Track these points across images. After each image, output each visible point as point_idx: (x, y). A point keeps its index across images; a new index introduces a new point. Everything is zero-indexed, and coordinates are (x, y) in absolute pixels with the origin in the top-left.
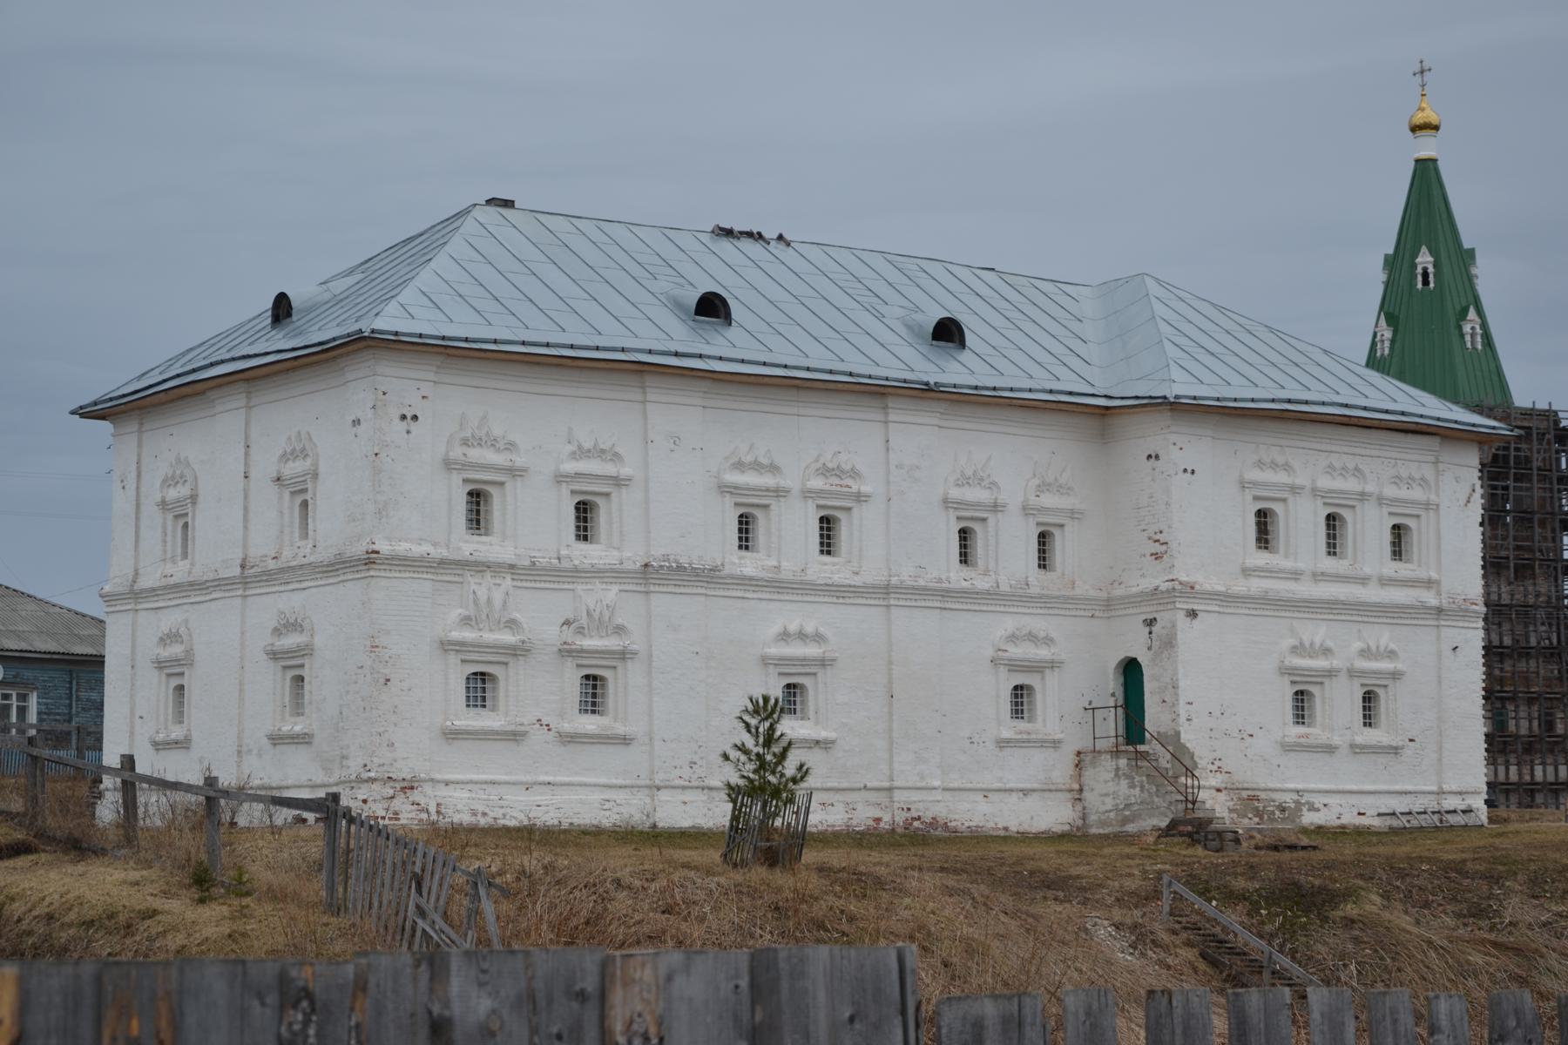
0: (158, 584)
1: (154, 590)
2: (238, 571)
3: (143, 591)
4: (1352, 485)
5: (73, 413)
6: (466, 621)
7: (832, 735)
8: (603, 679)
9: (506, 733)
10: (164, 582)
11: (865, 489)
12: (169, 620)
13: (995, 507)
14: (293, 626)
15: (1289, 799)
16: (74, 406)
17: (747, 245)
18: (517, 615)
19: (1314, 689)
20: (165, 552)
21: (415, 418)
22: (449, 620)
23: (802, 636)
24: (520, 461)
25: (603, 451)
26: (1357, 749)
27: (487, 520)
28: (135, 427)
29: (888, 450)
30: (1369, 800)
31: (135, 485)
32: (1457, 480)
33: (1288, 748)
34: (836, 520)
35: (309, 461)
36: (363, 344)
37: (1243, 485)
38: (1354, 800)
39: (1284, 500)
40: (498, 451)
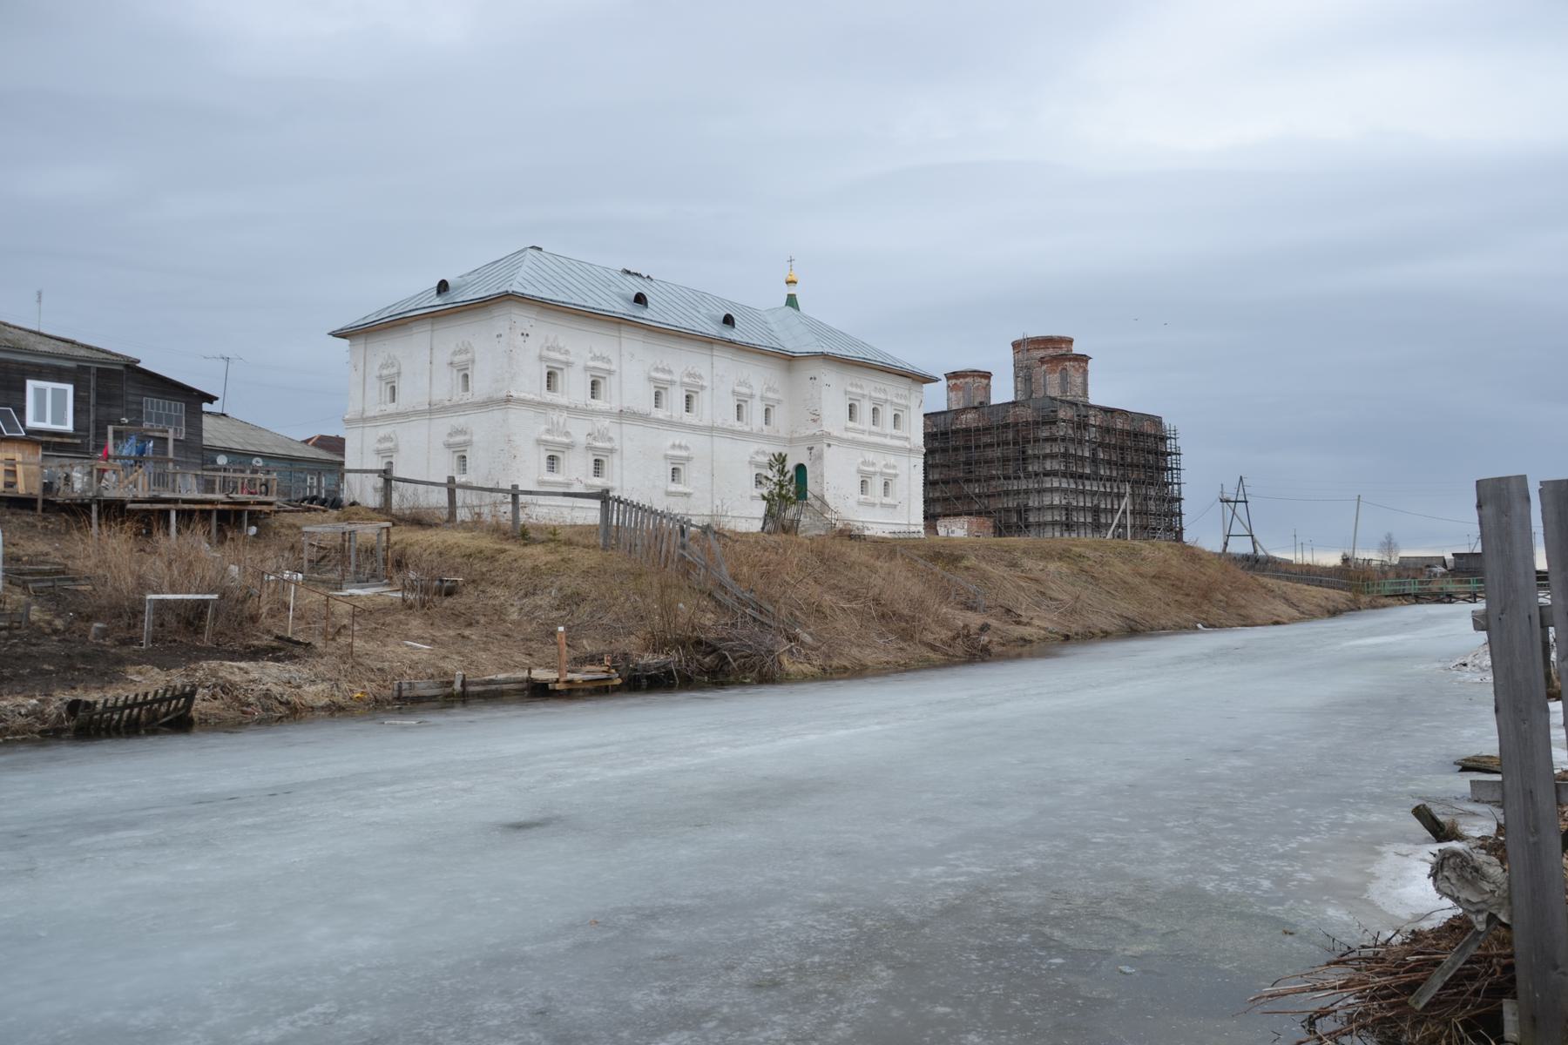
0: (376, 415)
1: (375, 417)
2: (427, 407)
3: (367, 418)
4: (882, 396)
5: (330, 334)
6: (548, 431)
7: (691, 491)
8: (602, 461)
9: (565, 483)
10: (381, 413)
11: (705, 384)
12: (382, 432)
13: (752, 396)
14: (462, 432)
15: (860, 525)
16: (330, 331)
17: (637, 278)
18: (569, 430)
19: (868, 480)
20: (381, 399)
21: (527, 335)
22: (540, 430)
23: (680, 447)
24: (571, 359)
25: (604, 358)
26: (883, 505)
27: (555, 386)
28: (363, 341)
29: (712, 367)
30: (887, 526)
31: (362, 368)
32: (916, 397)
33: (860, 503)
34: (692, 397)
35: (469, 355)
36: (507, 297)
37: (846, 393)
38: (881, 526)
39: (859, 400)
40: (562, 354)
